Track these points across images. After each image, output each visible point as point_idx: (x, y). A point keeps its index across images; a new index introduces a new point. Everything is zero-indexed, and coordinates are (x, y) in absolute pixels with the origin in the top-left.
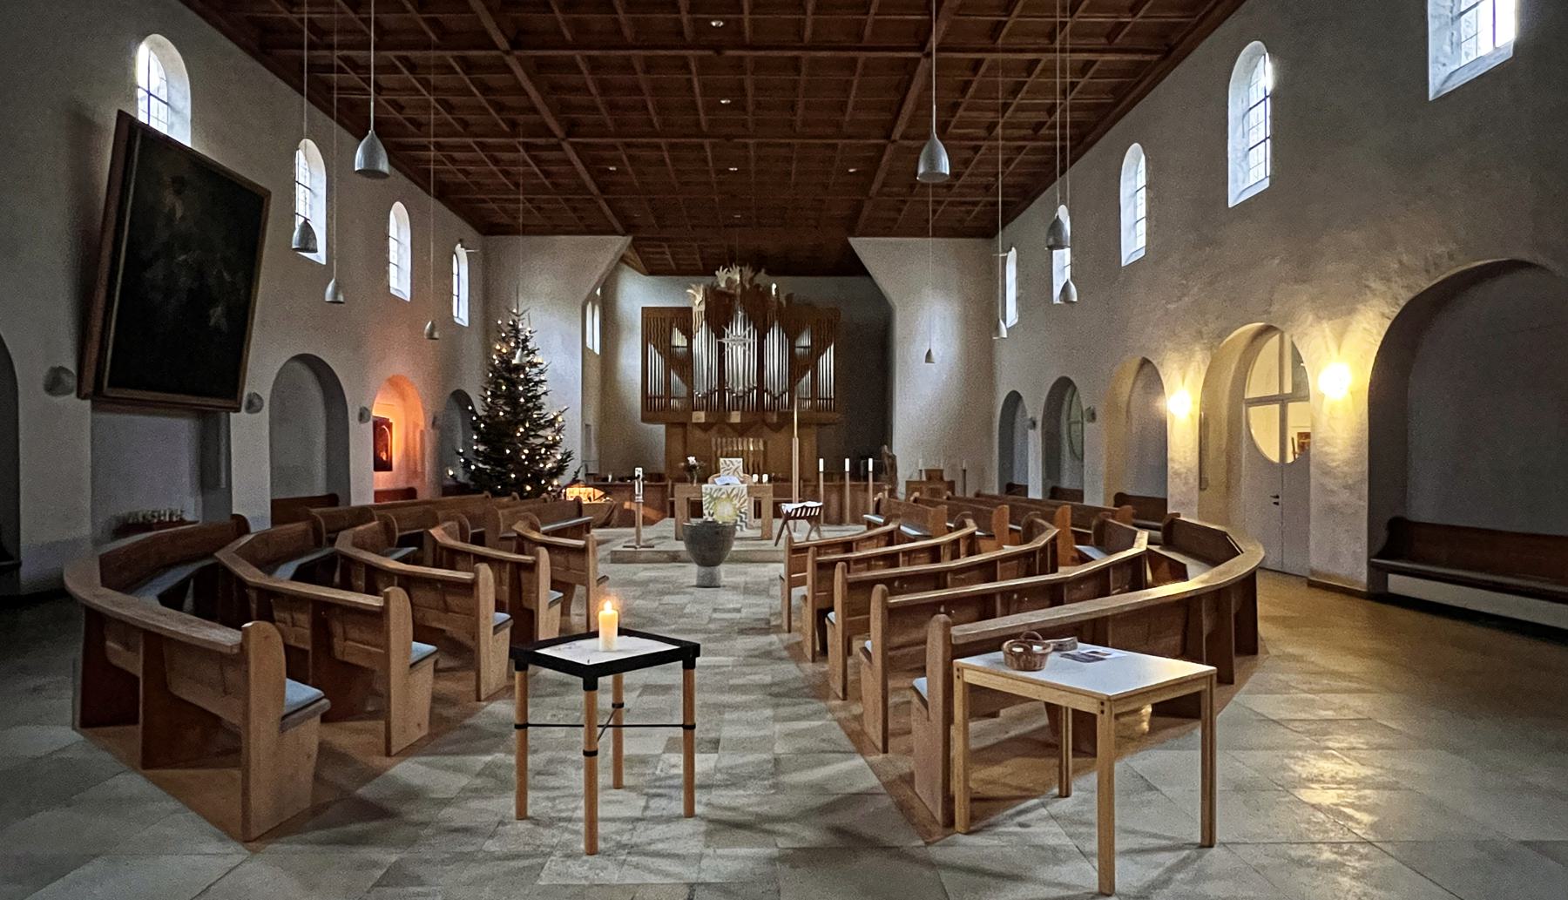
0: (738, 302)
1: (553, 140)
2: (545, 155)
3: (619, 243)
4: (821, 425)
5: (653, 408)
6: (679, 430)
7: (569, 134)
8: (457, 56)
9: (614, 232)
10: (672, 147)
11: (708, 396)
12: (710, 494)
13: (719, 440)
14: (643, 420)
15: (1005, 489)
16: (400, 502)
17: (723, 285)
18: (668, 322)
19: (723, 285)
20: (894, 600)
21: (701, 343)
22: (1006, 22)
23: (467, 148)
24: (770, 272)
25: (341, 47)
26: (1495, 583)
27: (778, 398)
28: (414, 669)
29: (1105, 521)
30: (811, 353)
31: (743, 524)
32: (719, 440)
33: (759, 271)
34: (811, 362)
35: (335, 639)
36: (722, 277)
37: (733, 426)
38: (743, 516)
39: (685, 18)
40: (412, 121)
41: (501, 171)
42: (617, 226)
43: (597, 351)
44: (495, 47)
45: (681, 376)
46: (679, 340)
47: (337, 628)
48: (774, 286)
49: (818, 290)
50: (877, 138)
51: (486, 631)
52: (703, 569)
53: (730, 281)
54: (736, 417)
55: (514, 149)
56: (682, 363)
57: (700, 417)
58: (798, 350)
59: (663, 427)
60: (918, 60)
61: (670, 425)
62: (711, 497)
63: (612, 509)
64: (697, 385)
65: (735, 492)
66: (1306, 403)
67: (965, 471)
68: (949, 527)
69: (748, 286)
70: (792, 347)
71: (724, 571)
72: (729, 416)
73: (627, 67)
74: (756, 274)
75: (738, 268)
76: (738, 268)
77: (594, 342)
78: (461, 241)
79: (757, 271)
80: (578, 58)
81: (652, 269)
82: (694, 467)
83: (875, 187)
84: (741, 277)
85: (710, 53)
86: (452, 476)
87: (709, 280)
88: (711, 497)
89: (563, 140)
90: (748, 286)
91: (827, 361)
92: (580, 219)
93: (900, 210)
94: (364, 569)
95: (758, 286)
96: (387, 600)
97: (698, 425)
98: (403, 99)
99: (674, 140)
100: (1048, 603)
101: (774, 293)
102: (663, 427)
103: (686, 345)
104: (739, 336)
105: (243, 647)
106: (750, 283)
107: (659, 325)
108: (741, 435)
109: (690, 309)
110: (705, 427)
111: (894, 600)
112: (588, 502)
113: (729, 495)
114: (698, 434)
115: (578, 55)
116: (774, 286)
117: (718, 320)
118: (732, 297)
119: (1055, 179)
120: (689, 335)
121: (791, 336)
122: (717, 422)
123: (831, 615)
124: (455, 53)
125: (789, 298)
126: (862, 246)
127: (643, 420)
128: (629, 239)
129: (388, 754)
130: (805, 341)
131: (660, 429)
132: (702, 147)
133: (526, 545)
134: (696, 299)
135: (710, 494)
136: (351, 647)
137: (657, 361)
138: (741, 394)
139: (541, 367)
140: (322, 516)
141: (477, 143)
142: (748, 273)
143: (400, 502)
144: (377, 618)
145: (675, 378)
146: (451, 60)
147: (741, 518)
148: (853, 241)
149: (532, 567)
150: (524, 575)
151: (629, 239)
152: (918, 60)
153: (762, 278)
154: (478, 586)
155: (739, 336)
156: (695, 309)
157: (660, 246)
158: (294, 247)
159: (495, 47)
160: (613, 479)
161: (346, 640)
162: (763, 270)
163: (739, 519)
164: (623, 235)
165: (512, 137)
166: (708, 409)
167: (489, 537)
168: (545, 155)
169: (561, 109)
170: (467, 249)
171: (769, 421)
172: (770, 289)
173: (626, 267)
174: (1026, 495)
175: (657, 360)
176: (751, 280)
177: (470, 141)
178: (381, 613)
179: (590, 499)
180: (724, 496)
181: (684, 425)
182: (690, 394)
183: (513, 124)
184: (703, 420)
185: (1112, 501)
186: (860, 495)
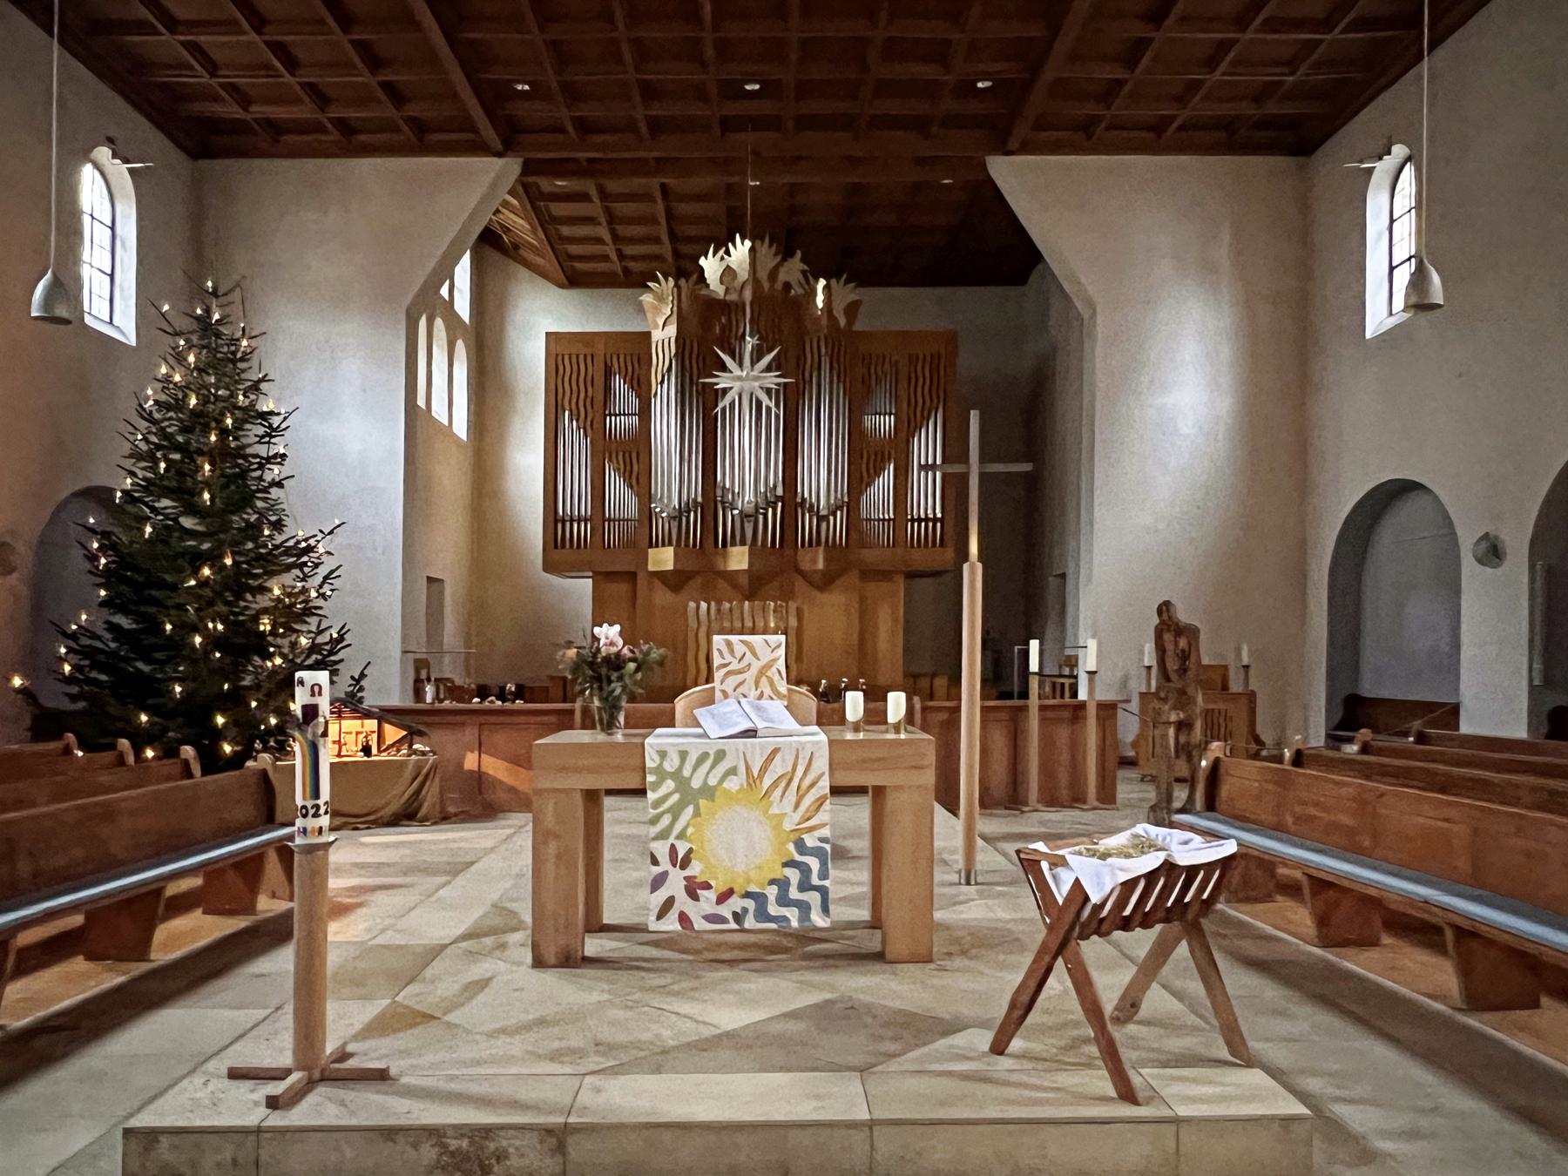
2: (558, 209)
4: (911, 576)
6: (622, 588)
9: (478, 148)
11: (680, 514)
12: (676, 775)
13: (704, 605)
14: (548, 566)
27: (826, 518)
31: (814, 898)
32: (704, 605)
34: (897, 451)
37: (731, 577)
38: (814, 863)
42: (490, 134)
43: (461, 428)
54: (738, 559)
57: (663, 558)
61: (603, 578)
62: (682, 784)
63: (423, 777)
64: (657, 487)
65: (779, 767)
67: (1247, 667)
72: (725, 556)
74: (784, 260)
76: (748, 243)
78: (110, 141)
79: (787, 254)
82: (616, 663)
86: (21, 691)
88: (682, 784)
95: (787, 286)
97: (661, 576)
108: (750, 596)
109: (648, 335)
110: (674, 581)
112: (361, 757)
113: (753, 781)
114: (662, 597)
118: (739, 307)
119: (1420, 58)
127: (548, 566)
128: (508, 168)
135: (676, 775)
138: (749, 508)
139: (276, 421)
142: (768, 258)
147: (805, 870)
151: (508, 168)
156: (657, 335)
158: (34, 314)
160: (437, 698)
162: (799, 254)
163: (794, 875)
164: (499, 155)
166: (680, 545)
170: (126, 161)
173: (524, 273)
174: (1457, 728)
175: (576, 446)
176: (773, 275)
179: (366, 750)
180: (733, 784)
181: (632, 576)
182: (647, 515)
184: (670, 566)
186: (1063, 734)
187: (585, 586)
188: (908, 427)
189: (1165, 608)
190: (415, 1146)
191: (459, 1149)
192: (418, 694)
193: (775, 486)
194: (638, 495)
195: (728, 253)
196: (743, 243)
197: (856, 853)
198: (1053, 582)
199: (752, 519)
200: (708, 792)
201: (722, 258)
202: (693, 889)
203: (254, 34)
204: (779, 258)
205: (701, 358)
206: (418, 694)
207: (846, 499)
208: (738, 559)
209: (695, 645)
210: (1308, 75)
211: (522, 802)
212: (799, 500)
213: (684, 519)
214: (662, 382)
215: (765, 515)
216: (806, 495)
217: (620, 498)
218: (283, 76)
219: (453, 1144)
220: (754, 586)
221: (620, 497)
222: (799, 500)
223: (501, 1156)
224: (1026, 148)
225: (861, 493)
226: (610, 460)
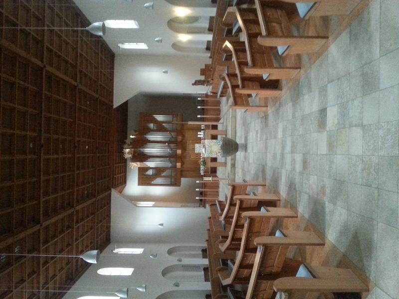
1: (75, 213)
2: (80, 217)
3: (114, 193)
5: (175, 183)
7: (73, 207)
9: (110, 195)
10: (78, 169)
11: (171, 162)
14: (179, 186)
15: (208, 51)
16: (210, 273)
17: (130, 156)
18: (143, 176)
19: (130, 156)
20: (264, 32)
21: (151, 164)
22: (33, 36)
23: (77, 244)
24: (126, 138)
25: (38, 288)
28: (286, 235)
35: (273, 271)
37: (182, 153)
39: (29, 157)
40: (67, 264)
41: (86, 234)
42: (109, 192)
44: (39, 230)
46: (150, 172)
47: (268, 270)
48: (131, 137)
49: (132, 122)
51: (267, 214)
52: (239, 149)
53: (129, 153)
54: (179, 152)
55: (78, 228)
56: (158, 171)
57: (179, 165)
58: (155, 128)
59: (182, 179)
60: (46, 71)
61: (182, 176)
68: (226, 59)
70: (154, 130)
71: (240, 140)
73: (47, 181)
77: (151, 204)
78: (112, 251)
80: (44, 199)
81: (124, 182)
83: (95, 95)
85: (42, 149)
91: (160, 118)
92: (105, 218)
94: (241, 270)
95: (131, 143)
96: (260, 244)
97: (182, 166)
98: (58, 267)
99: (75, 185)
101: (133, 137)
102: (182, 179)
104: (150, 150)
105: (285, 291)
107: (145, 179)
110: (183, 163)
111: (264, 32)
114: (185, 166)
115: (42, 199)
116: (131, 137)
117: (143, 157)
118: (135, 152)
120: (148, 168)
121: (149, 131)
122: (181, 159)
123: (265, 77)
125: (135, 131)
126: (117, 102)
128: (112, 190)
129: (323, 245)
130: (152, 126)
131: (183, 179)
132: (78, 158)
133: (230, 215)
134: (134, 166)
136: (276, 264)
137: (159, 180)
140: (215, 295)
141: (76, 241)
142: (126, 146)
143: (210, 273)
144: (267, 248)
146: (44, 247)
149: (241, 201)
150: (244, 206)
151: (112, 190)
152: (46, 71)
153: (128, 141)
154: (251, 216)
155: (150, 150)
156: (139, 166)
157: (116, 178)
159: (39, 230)
161: (274, 266)
165: (73, 228)
166: (176, 162)
168: (80, 217)
169: (63, 208)
171: (181, 140)
172: (132, 138)
176: (129, 145)
177: (74, 244)
178: (265, 246)
183: (69, 227)
184: (180, 164)
185: (215, 4)
187: (183, 179)
188: (155, 121)
189: (193, 84)
197: (248, 275)
200: (211, 151)
202: (219, 153)
208: (179, 152)
211: (211, 84)
220: (184, 149)
224: (112, 102)
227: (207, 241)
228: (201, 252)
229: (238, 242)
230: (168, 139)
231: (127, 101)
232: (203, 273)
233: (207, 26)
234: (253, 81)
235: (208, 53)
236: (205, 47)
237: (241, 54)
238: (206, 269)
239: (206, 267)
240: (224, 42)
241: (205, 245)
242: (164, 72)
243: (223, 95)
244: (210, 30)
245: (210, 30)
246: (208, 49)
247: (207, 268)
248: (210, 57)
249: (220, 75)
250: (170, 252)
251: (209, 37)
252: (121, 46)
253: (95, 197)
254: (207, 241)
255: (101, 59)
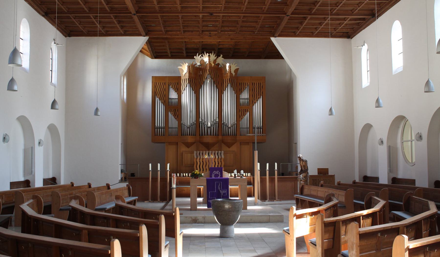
0: (207, 74)
8: (115, 16)
26: (205, 130)
29: (410, 196)
30: (249, 103)
33: (220, 56)
36: (198, 60)
42: (144, 33)
45: (175, 115)
46: (173, 95)
48: (228, 65)
50: (43, 200)
53: (202, 62)
66: (50, 108)
69: (213, 65)
70: (238, 98)
74: (217, 58)
75: (208, 54)
79: (218, 56)
84: (209, 60)
87: (190, 61)
89: (134, 14)
90: (213, 65)
93: (301, 23)
95: (218, 64)
100: (333, 217)
101: (227, 68)
103: (177, 97)
106: (214, 63)
116: (228, 65)
120: (179, 92)
121: (238, 91)
124: (93, 15)
125: (236, 71)
128: (146, 38)
130: (245, 95)
142: (213, 57)
145: (170, 115)
148: (273, 39)
151: (146, 38)
153: (220, 60)
162: (221, 56)
164: (144, 36)
167: (54, 209)
172: (225, 67)
176: (215, 61)
190: (189, 218)
191: (194, 219)
192: (211, 176)
193: (216, 119)
194: (178, 120)
195: (202, 56)
196: (206, 54)
198: (294, 145)
199: (210, 128)
201: (201, 57)
203: (93, 19)
204: (216, 57)
205: (195, 83)
206: (211, 176)
207: (236, 122)
209: (203, 167)
210: (344, 27)
212: (223, 122)
213: (191, 128)
214: (185, 90)
215: (192, 128)
216: (225, 122)
217: (173, 122)
218: (92, 19)
219: (193, 218)
221: (173, 122)
222: (223, 122)
223: (198, 219)
224: (280, 36)
225: (240, 121)
226: (170, 111)
227: (72, 184)
228: (51, 176)
229: (222, 197)
230: (225, 120)
231: (284, 59)
232: (22, 179)
233: (400, 176)
234: (333, 238)
235: (359, 180)
236: (369, 175)
237: (369, 221)
238: (27, 183)
239: (57, 181)
240: (384, 199)
241: (63, 181)
242: (331, 110)
243: (300, 204)
244: (395, 180)
245: (395, 180)
246: (366, 178)
247: (29, 186)
248: (354, 182)
249: (333, 195)
250: (52, 129)
251: (384, 180)
252: (365, 48)
253: (137, 12)
254: (72, 184)
255: (345, 19)
